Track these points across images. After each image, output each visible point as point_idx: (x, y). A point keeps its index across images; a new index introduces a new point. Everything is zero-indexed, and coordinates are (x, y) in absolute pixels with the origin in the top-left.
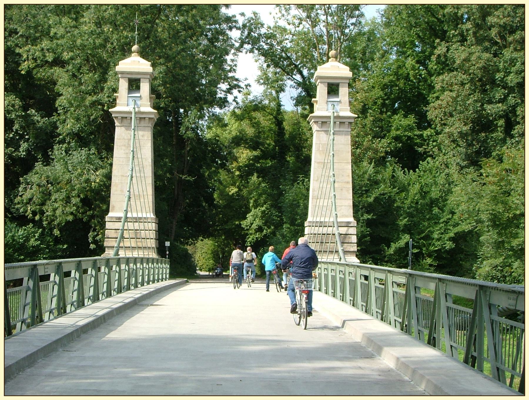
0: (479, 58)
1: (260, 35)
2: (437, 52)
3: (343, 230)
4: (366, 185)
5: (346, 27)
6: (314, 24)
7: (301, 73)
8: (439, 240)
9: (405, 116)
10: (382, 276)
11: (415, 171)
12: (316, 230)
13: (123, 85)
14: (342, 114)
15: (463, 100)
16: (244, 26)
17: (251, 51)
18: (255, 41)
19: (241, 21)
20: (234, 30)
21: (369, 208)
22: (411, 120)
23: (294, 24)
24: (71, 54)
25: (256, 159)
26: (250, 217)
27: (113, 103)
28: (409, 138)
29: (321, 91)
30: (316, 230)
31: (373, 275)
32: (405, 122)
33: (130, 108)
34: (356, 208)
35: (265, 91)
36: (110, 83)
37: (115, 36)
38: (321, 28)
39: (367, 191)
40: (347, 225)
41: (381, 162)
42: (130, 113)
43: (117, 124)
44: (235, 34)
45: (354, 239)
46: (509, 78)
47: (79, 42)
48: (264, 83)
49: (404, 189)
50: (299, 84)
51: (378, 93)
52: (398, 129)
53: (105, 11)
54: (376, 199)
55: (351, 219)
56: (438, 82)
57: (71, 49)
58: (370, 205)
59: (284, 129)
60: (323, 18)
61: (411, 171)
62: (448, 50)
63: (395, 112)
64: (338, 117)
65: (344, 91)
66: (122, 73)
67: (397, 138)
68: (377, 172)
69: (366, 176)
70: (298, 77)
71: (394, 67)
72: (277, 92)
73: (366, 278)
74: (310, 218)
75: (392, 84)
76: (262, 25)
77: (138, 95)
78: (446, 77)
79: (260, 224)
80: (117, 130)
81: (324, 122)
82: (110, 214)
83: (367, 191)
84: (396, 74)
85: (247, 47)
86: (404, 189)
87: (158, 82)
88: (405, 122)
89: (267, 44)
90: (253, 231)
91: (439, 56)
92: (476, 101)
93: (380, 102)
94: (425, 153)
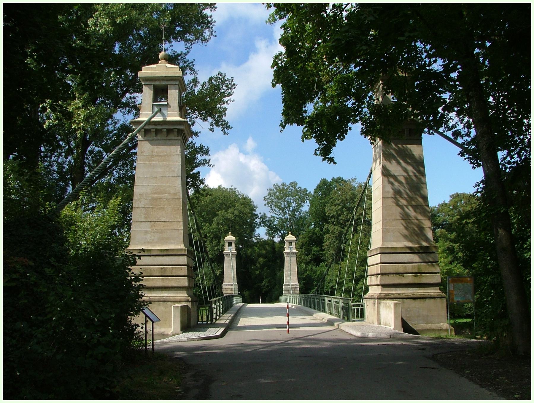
0: (337, 230)
1: (266, 220)
2: (325, 227)
3: (294, 286)
4: (303, 272)
5: (296, 215)
6: (285, 213)
7: (281, 233)
8: (327, 288)
9: (317, 247)
10: (336, 300)
11: (318, 266)
12: (286, 287)
13: (227, 244)
14: (293, 251)
15: (333, 243)
16: (261, 217)
17: (264, 226)
18: (265, 223)
19: (260, 216)
20: (257, 219)
21: (304, 279)
22: (318, 248)
23: (278, 215)
24: (209, 234)
25: (266, 262)
26: (264, 282)
27: (223, 250)
28: (318, 254)
29: (287, 244)
30: (286, 287)
31: (333, 300)
32: (316, 249)
33: (229, 251)
34: (299, 279)
35: (268, 238)
36: (222, 243)
37: (222, 229)
38: (287, 216)
39: (303, 273)
40: (296, 285)
41: (307, 264)
42: (229, 253)
43: (225, 256)
44: (258, 220)
45: (298, 289)
46: (347, 236)
47: (212, 231)
48: (268, 235)
49: (315, 272)
50: (280, 236)
51: (307, 239)
52: (314, 252)
53: (220, 221)
54: (306, 276)
55: (297, 283)
56: (326, 236)
57: (209, 233)
58: (304, 278)
59: (275, 251)
60: (288, 212)
61: (317, 267)
62: (328, 227)
63: (313, 246)
64: (292, 252)
65: (294, 244)
66: (226, 241)
67: (314, 255)
68: (306, 267)
69: (303, 269)
70: (280, 234)
71: (312, 231)
72: (273, 238)
73: (330, 301)
74: (284, 283)
75: (312, 236)
76: (267, 217)
77: (231, 247)
78: (328, 235)
79: (268, 284)
80: (225, 258)
81: (288, 253)
82: (224, 284)
83: (303, 273)
84: (313, 233)
85: (262, 224)
86: (315, 272)
87: (237, 242)
88: (316, 249)
89: (269, 223)
90: (265, 287)
91: (325, 228)
92: (337, 243)
93: (308, 242)
94: (323, 259)
